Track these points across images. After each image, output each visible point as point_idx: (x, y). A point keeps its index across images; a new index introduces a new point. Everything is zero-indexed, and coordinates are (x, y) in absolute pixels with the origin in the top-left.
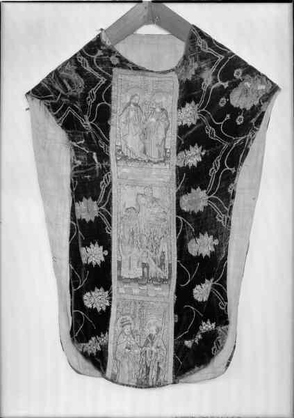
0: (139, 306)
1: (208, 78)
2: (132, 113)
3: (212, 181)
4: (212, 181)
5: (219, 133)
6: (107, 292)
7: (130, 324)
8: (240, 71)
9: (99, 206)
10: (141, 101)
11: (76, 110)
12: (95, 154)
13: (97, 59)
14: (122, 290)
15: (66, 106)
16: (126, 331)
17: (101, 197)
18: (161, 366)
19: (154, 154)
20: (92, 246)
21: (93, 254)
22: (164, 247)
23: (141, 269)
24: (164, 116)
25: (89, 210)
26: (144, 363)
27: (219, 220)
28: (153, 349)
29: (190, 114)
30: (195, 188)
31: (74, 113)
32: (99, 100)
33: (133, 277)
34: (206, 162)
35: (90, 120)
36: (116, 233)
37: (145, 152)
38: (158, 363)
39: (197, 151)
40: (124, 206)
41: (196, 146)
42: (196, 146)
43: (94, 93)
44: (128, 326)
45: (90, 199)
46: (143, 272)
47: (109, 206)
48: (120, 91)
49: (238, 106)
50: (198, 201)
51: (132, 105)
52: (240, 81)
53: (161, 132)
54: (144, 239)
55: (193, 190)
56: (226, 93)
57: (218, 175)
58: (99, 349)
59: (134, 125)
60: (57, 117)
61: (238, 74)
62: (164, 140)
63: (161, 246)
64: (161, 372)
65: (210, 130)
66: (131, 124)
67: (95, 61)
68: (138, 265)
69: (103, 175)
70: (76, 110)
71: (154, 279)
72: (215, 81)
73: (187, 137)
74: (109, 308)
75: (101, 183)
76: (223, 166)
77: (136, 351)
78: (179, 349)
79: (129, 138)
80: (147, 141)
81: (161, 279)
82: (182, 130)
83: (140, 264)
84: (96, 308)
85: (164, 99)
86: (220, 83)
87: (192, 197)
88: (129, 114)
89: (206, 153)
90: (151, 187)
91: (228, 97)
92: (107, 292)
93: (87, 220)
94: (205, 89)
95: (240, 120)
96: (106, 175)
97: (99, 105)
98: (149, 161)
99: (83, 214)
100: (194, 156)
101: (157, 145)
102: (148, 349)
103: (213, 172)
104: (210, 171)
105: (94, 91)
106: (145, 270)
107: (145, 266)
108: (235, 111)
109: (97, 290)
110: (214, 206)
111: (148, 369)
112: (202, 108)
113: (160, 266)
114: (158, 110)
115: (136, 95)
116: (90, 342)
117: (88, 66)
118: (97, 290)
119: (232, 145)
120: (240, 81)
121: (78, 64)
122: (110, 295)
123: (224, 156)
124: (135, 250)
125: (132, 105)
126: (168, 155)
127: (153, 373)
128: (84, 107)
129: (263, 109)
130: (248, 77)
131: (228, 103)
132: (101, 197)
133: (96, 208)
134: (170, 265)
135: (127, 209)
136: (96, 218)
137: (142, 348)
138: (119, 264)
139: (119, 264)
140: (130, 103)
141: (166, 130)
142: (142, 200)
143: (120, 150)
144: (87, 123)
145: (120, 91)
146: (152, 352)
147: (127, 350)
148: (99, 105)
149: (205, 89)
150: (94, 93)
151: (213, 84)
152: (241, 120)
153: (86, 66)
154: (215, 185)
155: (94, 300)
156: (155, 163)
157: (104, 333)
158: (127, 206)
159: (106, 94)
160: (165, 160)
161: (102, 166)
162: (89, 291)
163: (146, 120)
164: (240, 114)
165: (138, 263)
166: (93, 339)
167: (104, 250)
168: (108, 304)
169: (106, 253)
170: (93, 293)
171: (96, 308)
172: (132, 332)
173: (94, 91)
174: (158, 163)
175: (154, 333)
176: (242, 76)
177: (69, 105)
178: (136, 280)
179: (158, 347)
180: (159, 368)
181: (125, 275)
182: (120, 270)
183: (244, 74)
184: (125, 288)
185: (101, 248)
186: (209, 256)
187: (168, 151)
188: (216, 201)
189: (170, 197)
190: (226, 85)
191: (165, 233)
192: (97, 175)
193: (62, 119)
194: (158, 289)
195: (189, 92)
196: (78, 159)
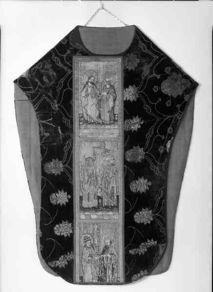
0: (96, 227)
1: (146, 70)
2: (90, 90)
3: (148, 142)
4: (148, 142)
5: (153, 111)
6: (70, 224)
7: (91, 240)
8: (169, 68)
9: (64, 164)
10: (96, 80)
11: (49, 97)
12: (59, 127)
13: (66, 57)
14: (83, 217)
15: (41, 96)
16: (88, 245)
17: (65, 157)
18: (115, 267)
19: (106, 117)
20: (59, 192)
21: (60, 198)
22: (113, 184)
23: (97, 200)
24: (113, 90)
25: (55, 167)
26: (102, 266)
27: (152, 169)
28: (109, 255)
29: (131, 94)
30: (136, 146)
31: (47, 99)
32: (65, 87)
33: (91, 207)
34: (144, 128)
35: (58, 102)
36: (79, 178)
37: (100, 117)
38: (113, 265)
39: (138, 121)
40: (84, 156)
41: (137, 117)
42: (137, 117)
43: (62, 82)
44: (89, 242)
45: (57, 160)
46: (98, 202)
47: (71, 164)
48: (80, 74)
49: (166, 94)
50: (138, 154)
51: (89, 84)
52: (168, 75)
53: (111, 104)
54: (99, 179)
55: (134, 147)
56: (159, 83)
57: (152, 138)
58: (66, 263)
59: (92, 97)
60: (34, 103)
61: (167, 70)
62: (113, 108)
63: (112, 183)
64: (115, 271)
65: (147, 107)
66: (89, 97)
67: (65, 58)
68: (94, 198)
69: (66, 142)
70: (49, 97)
71: (107, 207)
72: (151, 73)
73: (130, 109)
74: (72, 235)
75: (65, 148)
76: (155, 133)
77: (97, 258)
78: (128, 258)
79: (88, 108)
80: (101, 109)
81: (111, 206)
82: (127, 104)
83: (96, 197)
84: (63, 235)
85: (111, 79)
86: (154, 74)
87: (133, 152)
88: (87, 90)
89: (144, 123)
90: (104, 142)
91: (160, 86)
92: (70, 224)
93: (56, 174)
94: (143, 78)
95: (168, 104)
96: (67, 142)
97: (65, 90)
98: (103, 123)
99: (52, 170)
100: (136, 124)
101: (109, 112)
102: (105, 256)
103: (148, 136)
104: (147, 135)
105: (62, 80)
106: (100, 201)
107: (99, 198)
108: (165, 97)
109: (63, 222)
110: (150, 161)
111: (105, 269)
112: (141, 90)
113: (110, 198)
114: (108, 86)
115: (92, 76)
116: (60, 259)
117: (60, 63)
118: (63, 222)
119: (162, 120)
120: (168, 75)
121: (53, 62)
122: (73, 226)
123: (156, 127)
124: (93, 187)
125: (89, 84)
126: (116, 119)
127: (109, 272)
128: (54, 95)
129: (186, 98)
130: (174, 74)
131: (160, 91)
132: (65, 157)
133: (61, 165)
134: (118, 197)
135: (86, 159)
136: (62, 172)
137: (100, 255)
138: (81, 198)
139: (81, 198)
140: (87, 83)
141: (115, 100)
142: (99, 151)
143: (83, 117)
144: (55, 106)
145: (80, 74)
146: (108, 257)
147: (90, 258)
148: (65, 90)
149: (143, 78)
150: (62, 82)
151: (150, 75)
152: (169, 103)
153: (58, 64)
154: (150, 144)
155: (62, 229)
156: (107, 124)
157: (70, 252)
158: (86, 157)
159: (69, 82)
160: (114, 121)
161: (65, 135)
162: (58, 224)
163: (100, 94)
164: (169, 100)
165: (94, 197)
166: (62, 257)
167: (67, 195)
168: (71, 232)
169: (70, 197)
170: (61, 225)
171: (63, 235)
172: (92, 246)
173: (62, 80)
174: (110, 124)
175: (109, 244)
176: (170, 72)
177: (43, 93)
178: (94, 208)
179: (112, 254)
180: (113, 268)
181: (85, 204)
182: (82, 202)
183: (172, 71)
184: (86, 215)
185: (66, 193)
186: (145, 193)
187: (116, 116)
188: (150, 156)
189: (118, 149)
190: (159, 77)
191: (115, 174)
192: (62, 142)
193: (38, 104)
194: (111, 213)
195: (129, 79)
196: (46, 132)
